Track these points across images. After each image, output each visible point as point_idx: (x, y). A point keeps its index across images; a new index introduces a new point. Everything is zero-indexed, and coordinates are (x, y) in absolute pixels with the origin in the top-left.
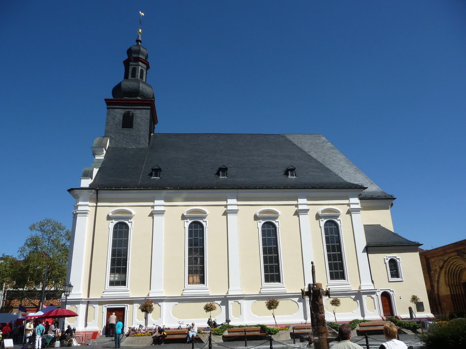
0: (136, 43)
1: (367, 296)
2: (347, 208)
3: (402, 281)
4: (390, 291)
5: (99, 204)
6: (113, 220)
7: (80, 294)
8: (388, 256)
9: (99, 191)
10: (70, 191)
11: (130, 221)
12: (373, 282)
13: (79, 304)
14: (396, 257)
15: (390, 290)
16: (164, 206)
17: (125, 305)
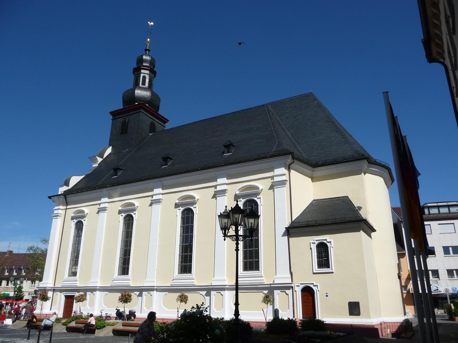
0: (145, 51)
1: (281, 292)
2: (269, 182)
3: (332, 273)
4: (314, 286)
5: (68, 207)
6: (180, 207)
7: (225, 280)
8: (315, 239)
9: (67, 196)
10: (50, 197)
11: (194, 206)
12: (291, 273)
13: (154, 291)
14: (326, 240)
15: (313, 284)
16: (227, 184)
17: (75, 293)
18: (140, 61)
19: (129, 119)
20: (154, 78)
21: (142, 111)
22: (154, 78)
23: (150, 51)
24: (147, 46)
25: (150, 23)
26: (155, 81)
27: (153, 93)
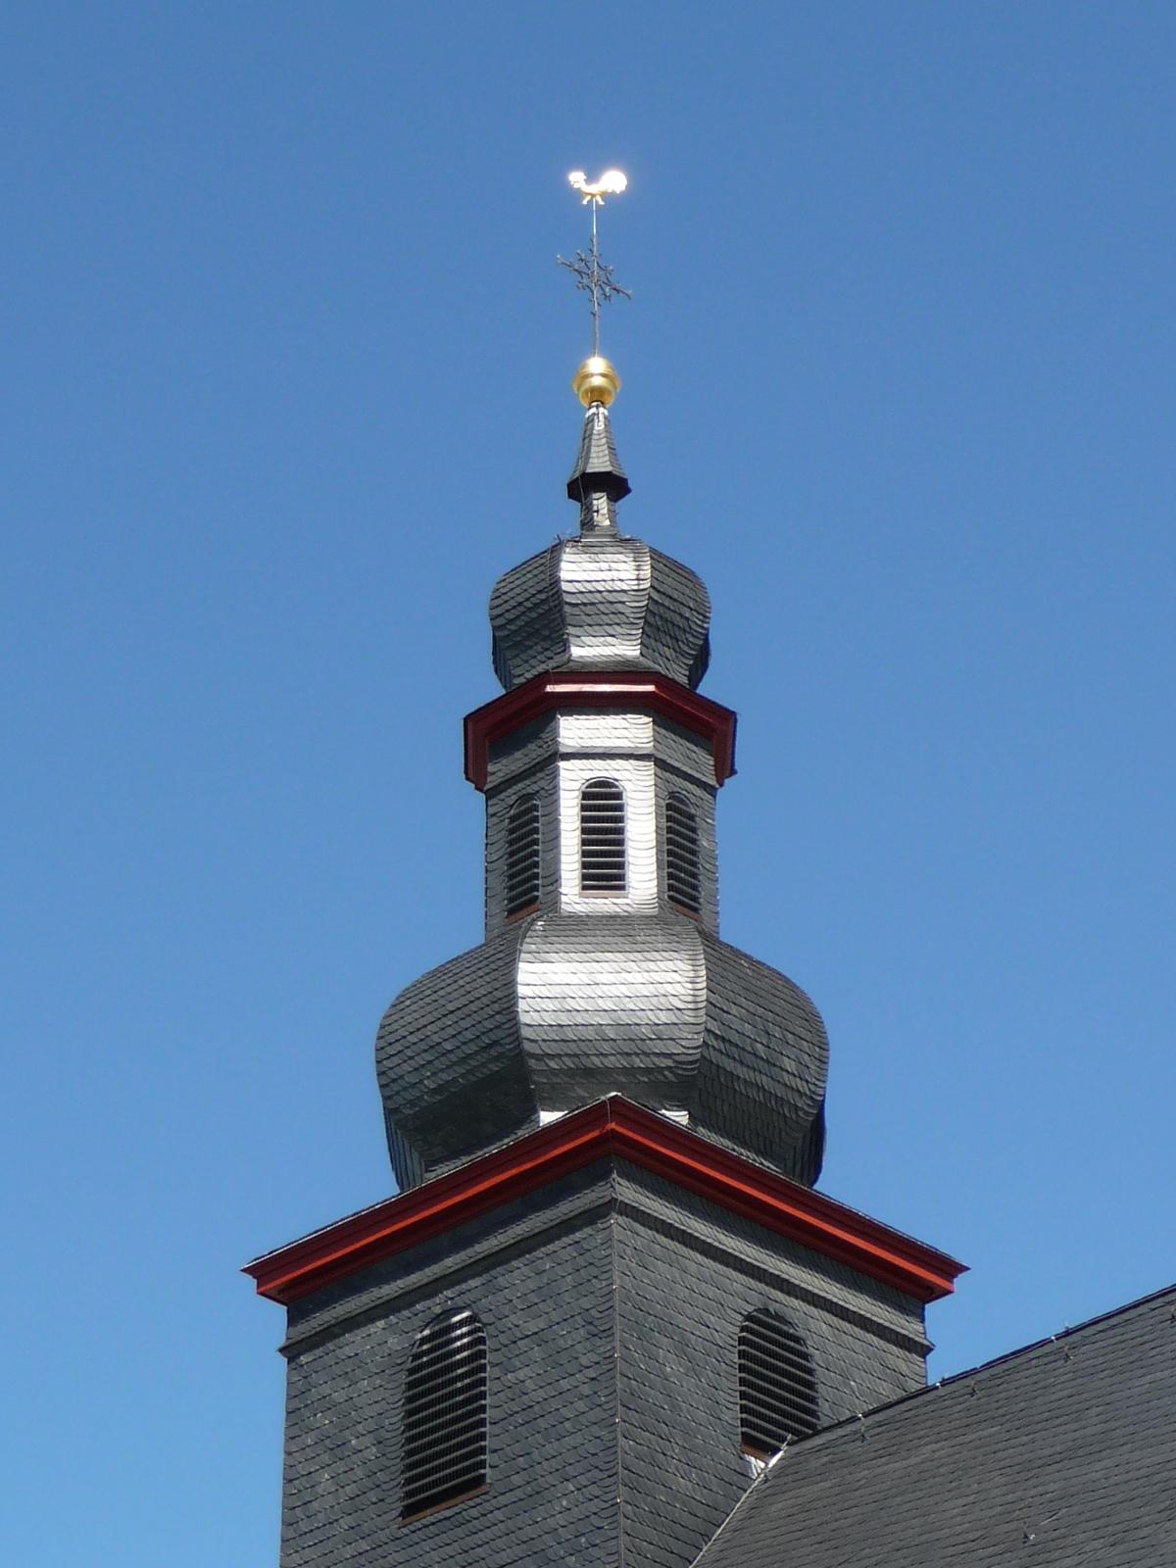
0: (575, 506)
18: (532, 619)
19: (484, 1318)
20: (712, 791)
21: (627, 1191)
22: (712, 791)
23: (627, 491)
24: (587, 436)
25: (591, 178)
26: (732, 821)
27: (725, 964)
